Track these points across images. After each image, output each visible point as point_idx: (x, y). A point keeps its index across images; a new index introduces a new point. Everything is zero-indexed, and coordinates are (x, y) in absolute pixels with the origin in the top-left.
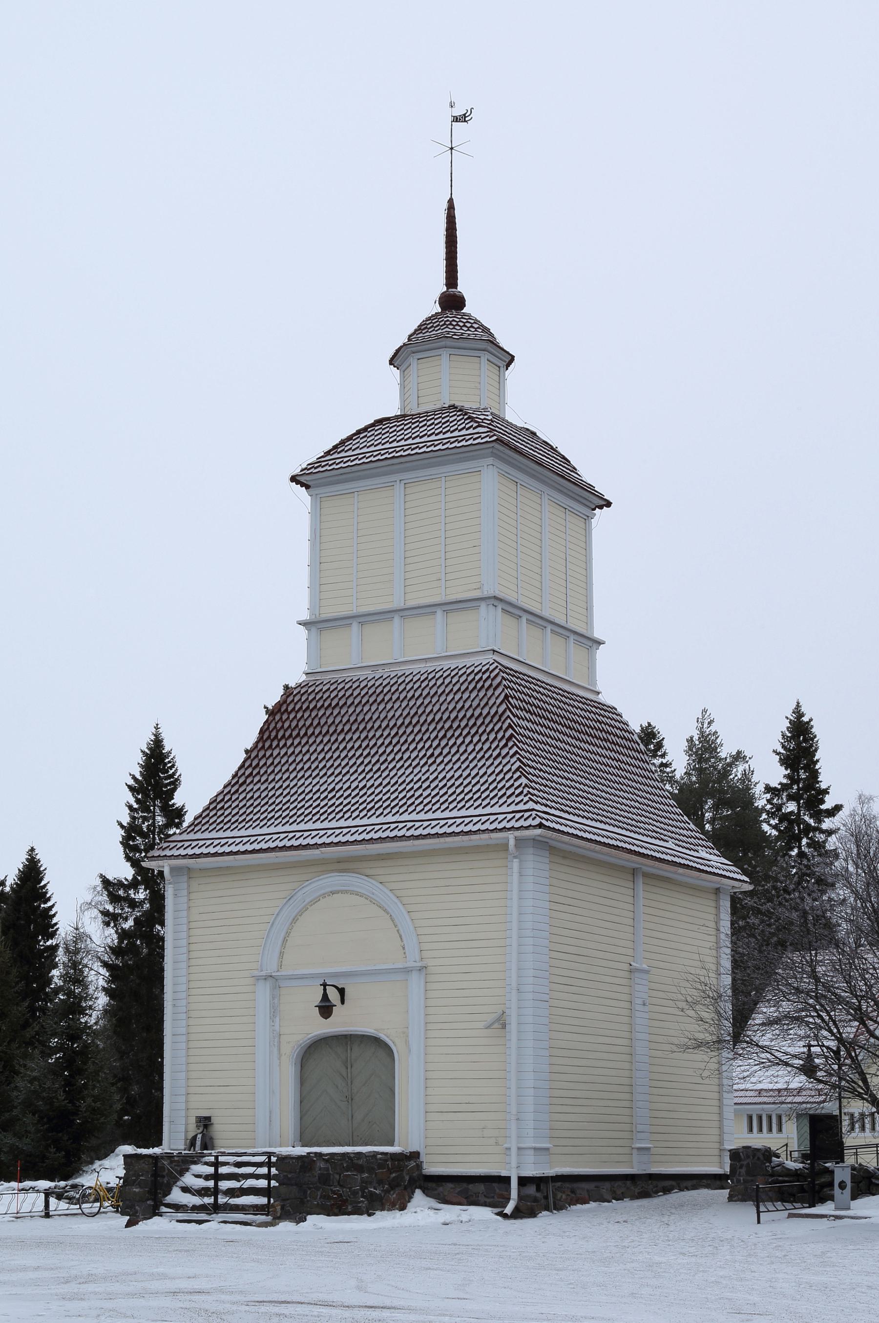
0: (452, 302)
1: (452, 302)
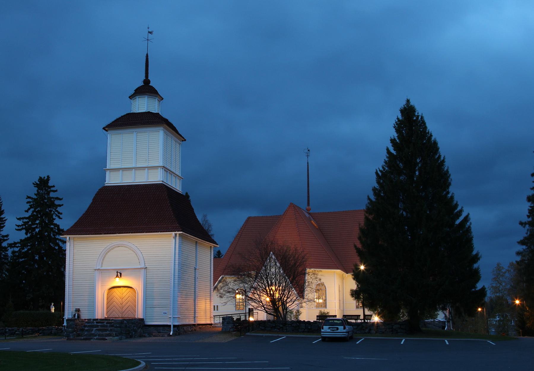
0: (147, 82)
1: (147, 82)
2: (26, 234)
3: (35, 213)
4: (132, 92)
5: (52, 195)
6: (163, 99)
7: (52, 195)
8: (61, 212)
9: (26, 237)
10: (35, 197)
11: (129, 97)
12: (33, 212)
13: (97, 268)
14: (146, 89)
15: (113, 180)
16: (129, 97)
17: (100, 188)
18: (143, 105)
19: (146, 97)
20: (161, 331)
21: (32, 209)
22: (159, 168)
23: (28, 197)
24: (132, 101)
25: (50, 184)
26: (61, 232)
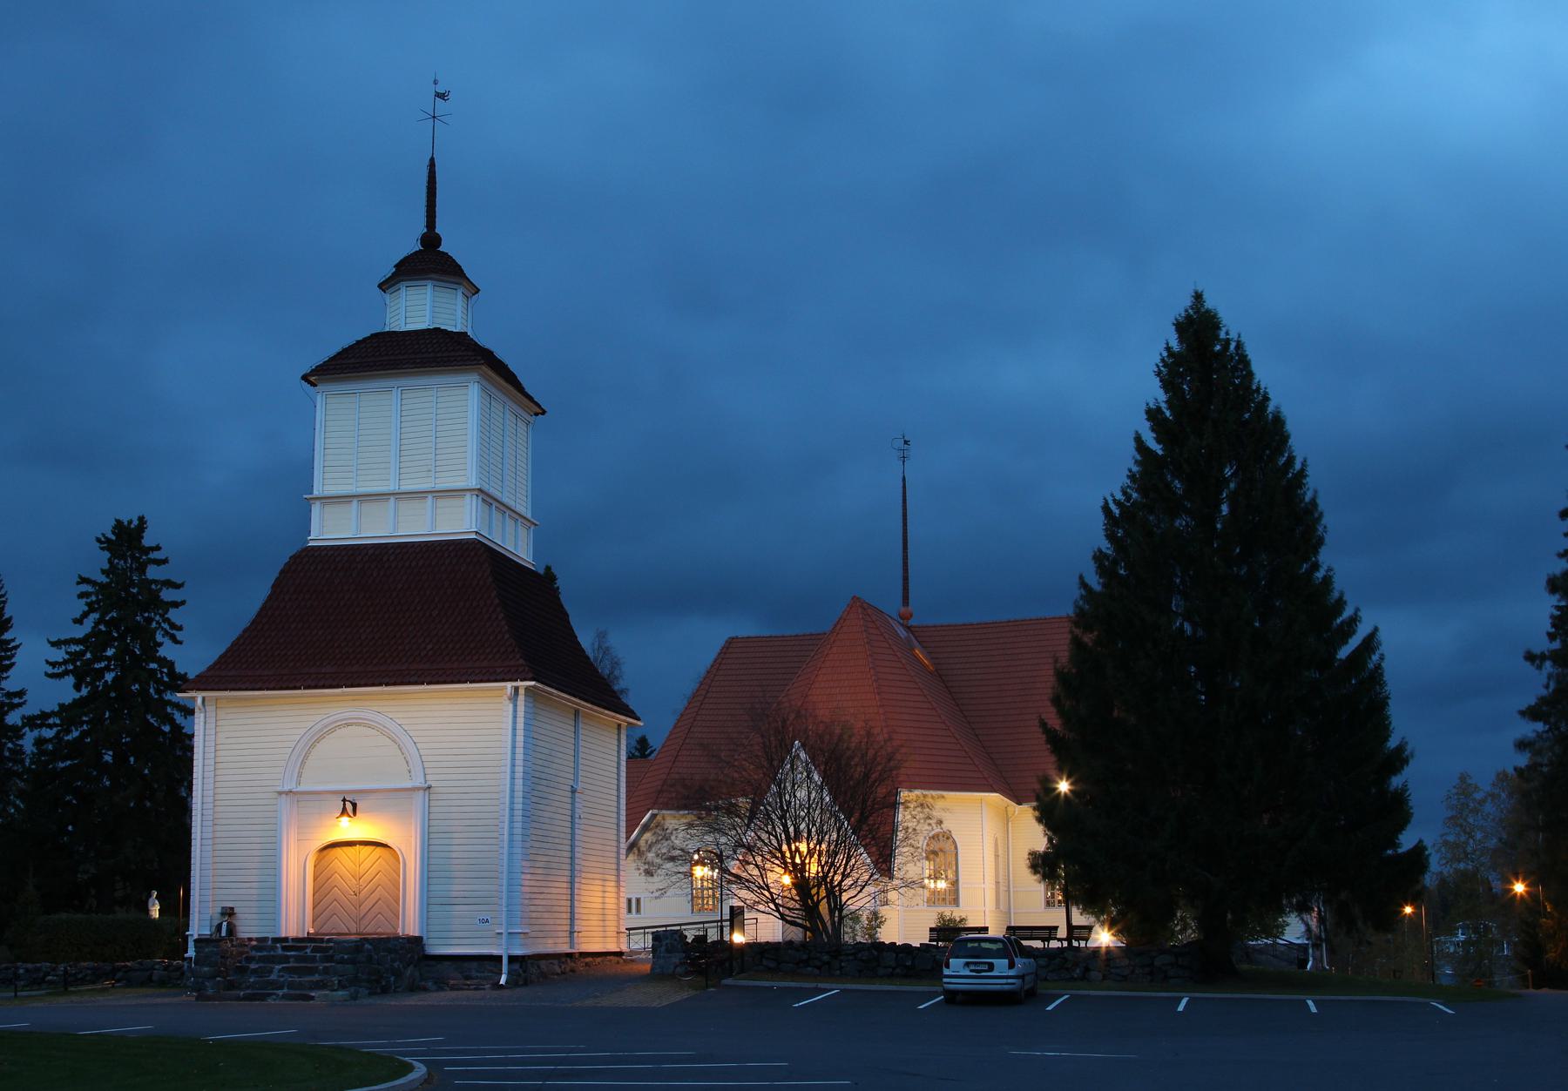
0: (431, 240)
1: (431, 240)
2: (77, 687)
3: (102, 627)
4: (389, 270)
5: (153, 572)
6: (478, 291)
7: (153, 572)
8: (178, 623)
9: (77, 695)
10: (103, 579)
11: (380, 286)
12: (97, 623)
13: (286, 788)
14: (429, 262)
15: (331, 528)
16: (380, 286)
17: (292, 551)
18: (419, 309)
19: (430, 284)
20: (474, 974)
21: (95, 616)
22: (468, 495)
23: (83, 580)
24: (387, 296)
25: (147, 541)
26: (180, 682)
